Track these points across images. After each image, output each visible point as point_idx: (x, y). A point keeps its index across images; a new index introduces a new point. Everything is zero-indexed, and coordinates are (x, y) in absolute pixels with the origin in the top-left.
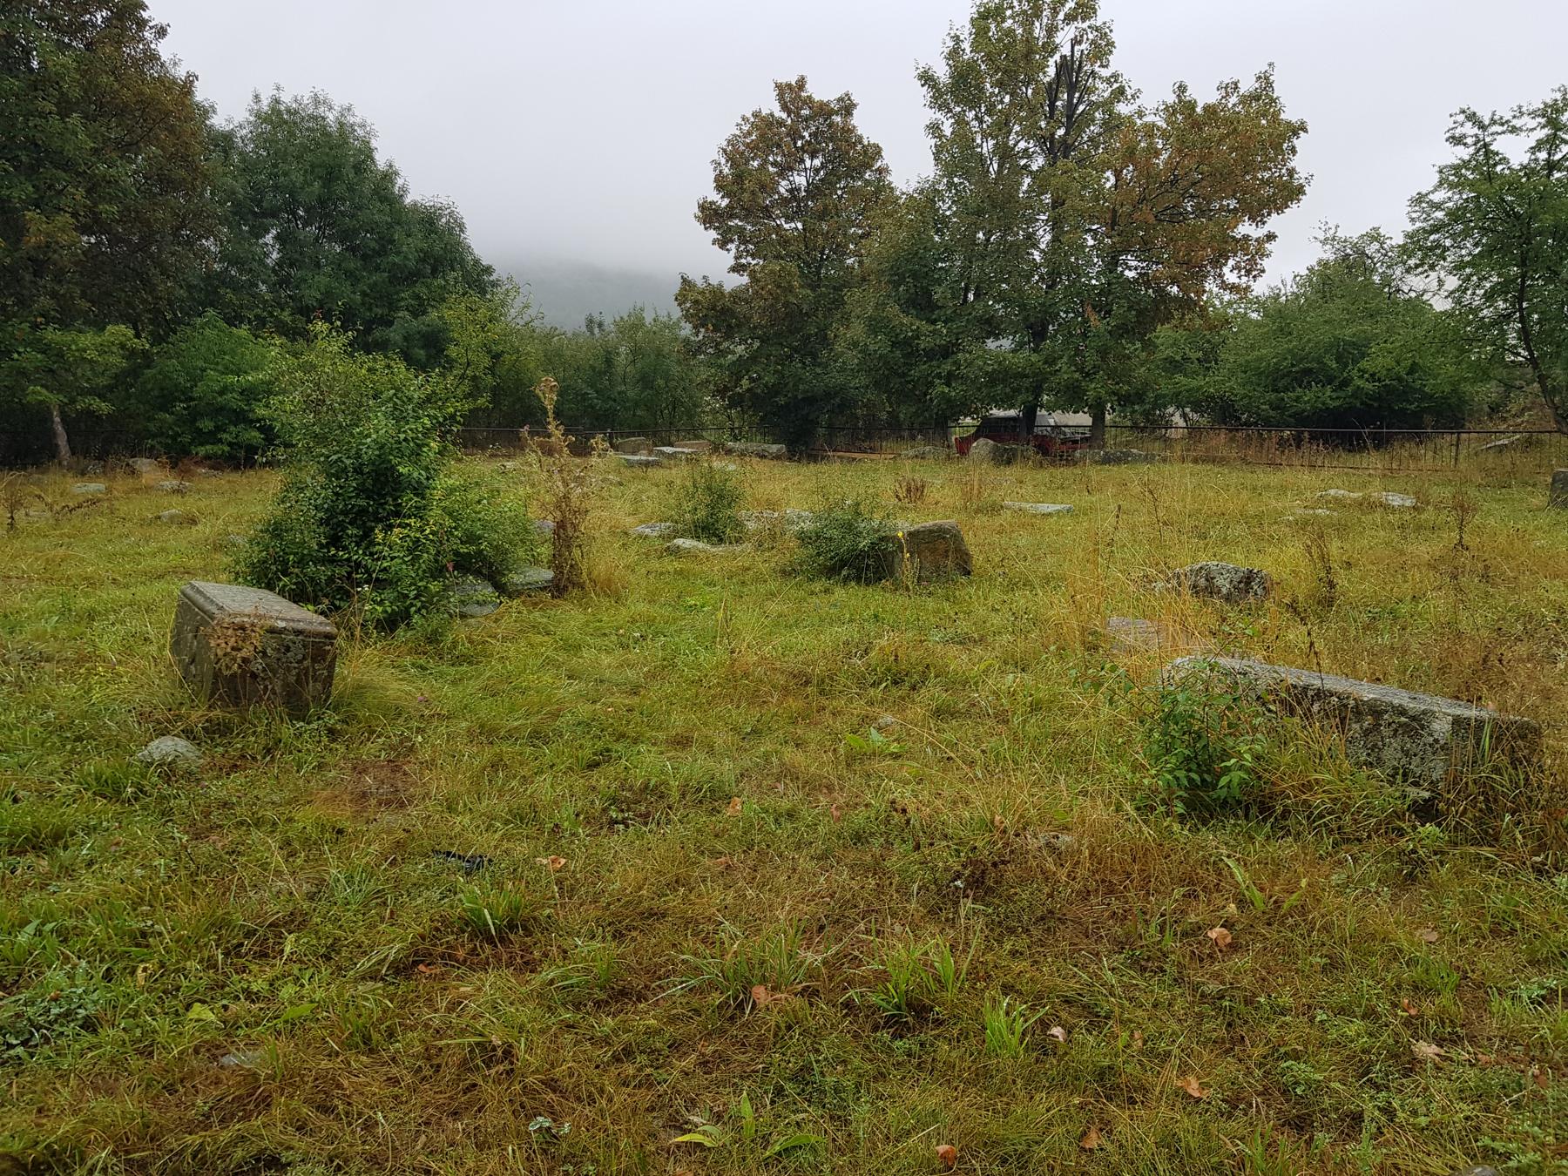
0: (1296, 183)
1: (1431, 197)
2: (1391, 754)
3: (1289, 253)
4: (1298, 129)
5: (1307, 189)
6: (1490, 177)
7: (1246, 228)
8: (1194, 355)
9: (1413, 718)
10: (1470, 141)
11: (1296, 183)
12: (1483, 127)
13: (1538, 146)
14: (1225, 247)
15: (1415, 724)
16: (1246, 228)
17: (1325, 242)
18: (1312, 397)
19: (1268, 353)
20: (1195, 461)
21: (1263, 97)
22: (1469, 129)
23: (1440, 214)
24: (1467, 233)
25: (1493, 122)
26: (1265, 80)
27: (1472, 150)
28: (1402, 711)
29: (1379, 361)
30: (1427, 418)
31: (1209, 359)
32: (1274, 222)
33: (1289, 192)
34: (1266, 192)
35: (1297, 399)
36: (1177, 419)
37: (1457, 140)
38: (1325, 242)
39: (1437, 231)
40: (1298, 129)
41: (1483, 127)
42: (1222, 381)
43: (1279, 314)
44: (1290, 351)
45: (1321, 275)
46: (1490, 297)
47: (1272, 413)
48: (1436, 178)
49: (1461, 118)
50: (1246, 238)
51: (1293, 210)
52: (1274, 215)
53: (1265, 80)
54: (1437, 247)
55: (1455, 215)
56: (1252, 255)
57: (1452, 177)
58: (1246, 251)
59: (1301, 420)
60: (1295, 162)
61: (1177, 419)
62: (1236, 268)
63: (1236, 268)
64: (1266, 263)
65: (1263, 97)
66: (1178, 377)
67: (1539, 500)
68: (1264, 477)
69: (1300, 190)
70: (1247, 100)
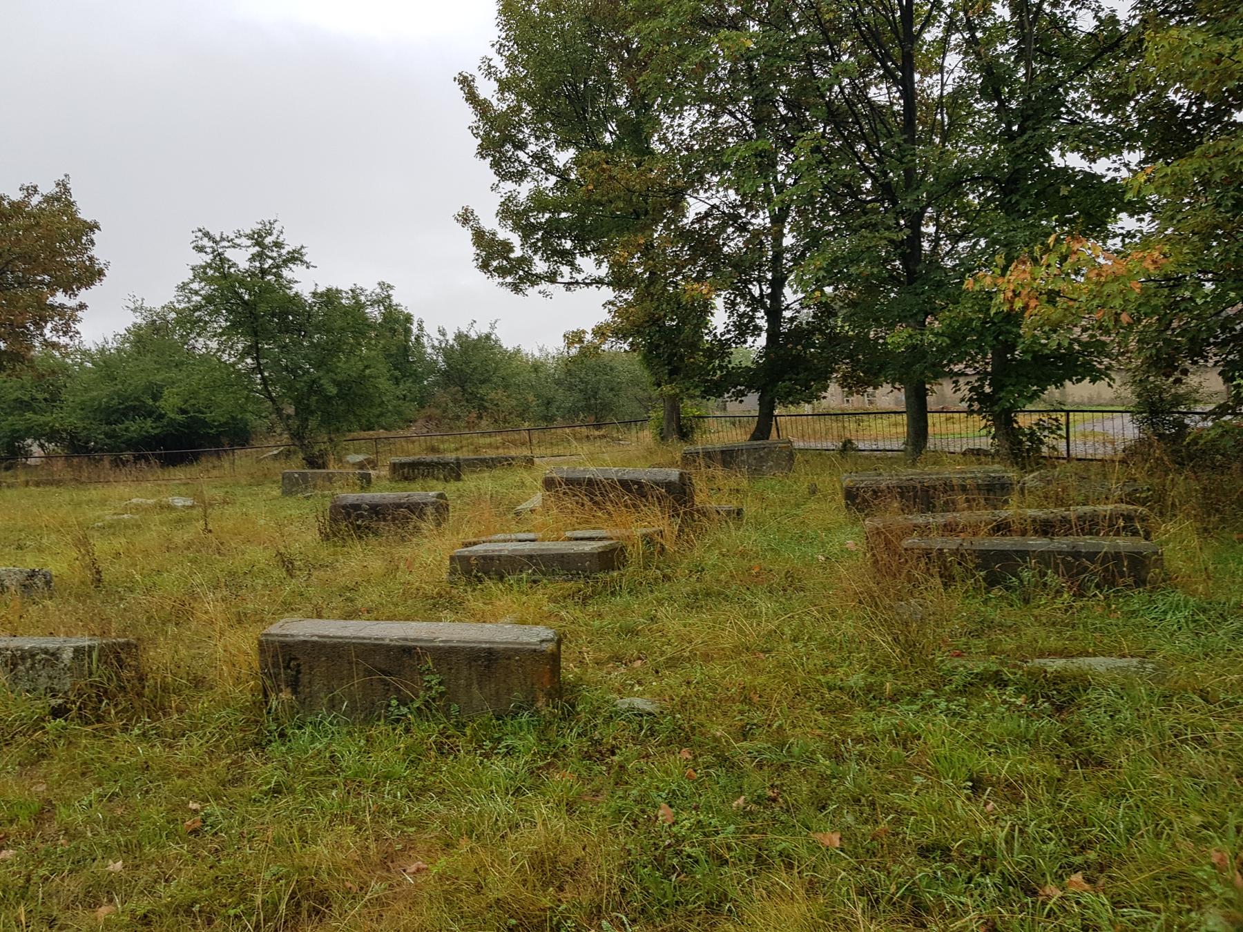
0: (97, 267)
1: (945, 93)
2: (43, 682)
3: (100, 322)
4: (93, 227)
5: (106, 272)
6: (225, 276)
7: (60, 298)
8: (40, 396)
9: (53, 654)
10: (209, 250)
11: (97, 267)
12: (215, 242)
13: (253, 259)
14: (44, 313)
15: (54, 655)
16: (60, 298)
17: (135, 310)
18: (134, 427)
19: (103, 393)
20: (37, 484)
21: (61, 200)
22: (206, 242)
23: (196, 298)
24: (217, 312)
25: (222, 239)
26: (63, 186)
27: (211, 256)
28: (46, 651)
29: (170, 403)
30: (225, 440)
31: (54, 399)
32: (84, 295)
33: (91, 275)
34: (75, 272)
35: (127, 429)
36: (35, 449)
37: (201, 249)
38: (135, 310)
39: (199, 310)
40: (93, 227)
41: (215, 242)
42: (65, 418)
43: (107, 364)
44: (116, 393)
45: (137, 335)
46: (242, 356)
47: (107, 441)
48: (191, 274)
49: (200, 234)
50: (62, 306)
51: (97, 288)
52: (83, 290)
53: (63, 186)
54: (200, 320)
55: (209, 299)
56: (67, 318)
57: (200, 273)
58: (62, 317)
59: (131, 444)
60: (95, 252)
61: (35, 449)
62: (54, 329)
63: (54, 329)
64: (78, 327)
65: (61, 200)
66: (28, 415)
67: (277, 492)
68: (95, 493)
69: (101, 273)
70: (49, 199)
